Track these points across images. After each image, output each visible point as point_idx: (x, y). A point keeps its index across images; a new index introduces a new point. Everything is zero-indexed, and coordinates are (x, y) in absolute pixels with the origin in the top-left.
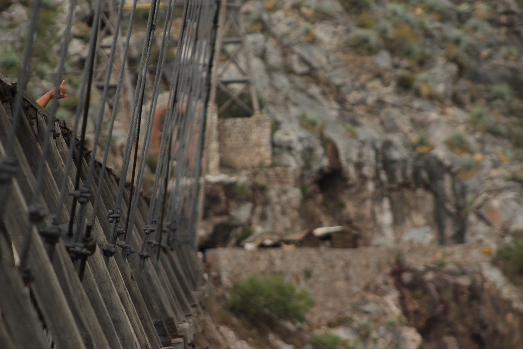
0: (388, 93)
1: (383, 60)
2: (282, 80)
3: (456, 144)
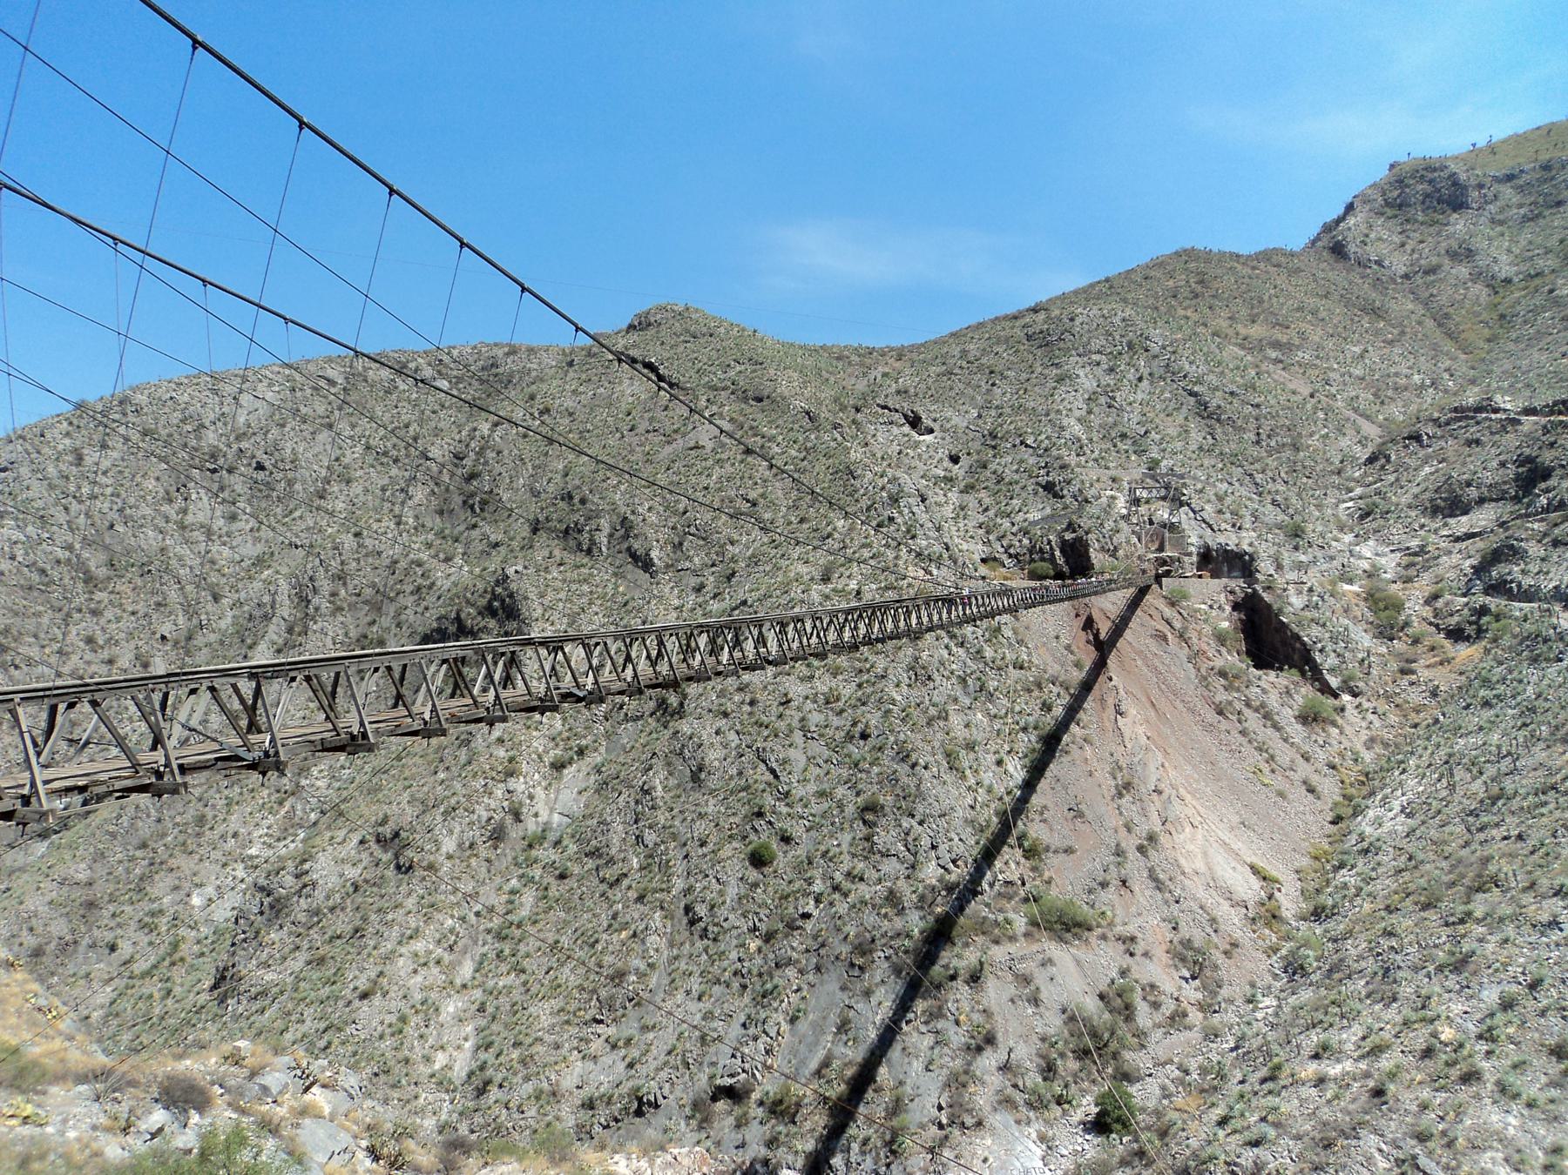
0: (1229, 527)
1: (1228, 516)
3: (1251, 545)
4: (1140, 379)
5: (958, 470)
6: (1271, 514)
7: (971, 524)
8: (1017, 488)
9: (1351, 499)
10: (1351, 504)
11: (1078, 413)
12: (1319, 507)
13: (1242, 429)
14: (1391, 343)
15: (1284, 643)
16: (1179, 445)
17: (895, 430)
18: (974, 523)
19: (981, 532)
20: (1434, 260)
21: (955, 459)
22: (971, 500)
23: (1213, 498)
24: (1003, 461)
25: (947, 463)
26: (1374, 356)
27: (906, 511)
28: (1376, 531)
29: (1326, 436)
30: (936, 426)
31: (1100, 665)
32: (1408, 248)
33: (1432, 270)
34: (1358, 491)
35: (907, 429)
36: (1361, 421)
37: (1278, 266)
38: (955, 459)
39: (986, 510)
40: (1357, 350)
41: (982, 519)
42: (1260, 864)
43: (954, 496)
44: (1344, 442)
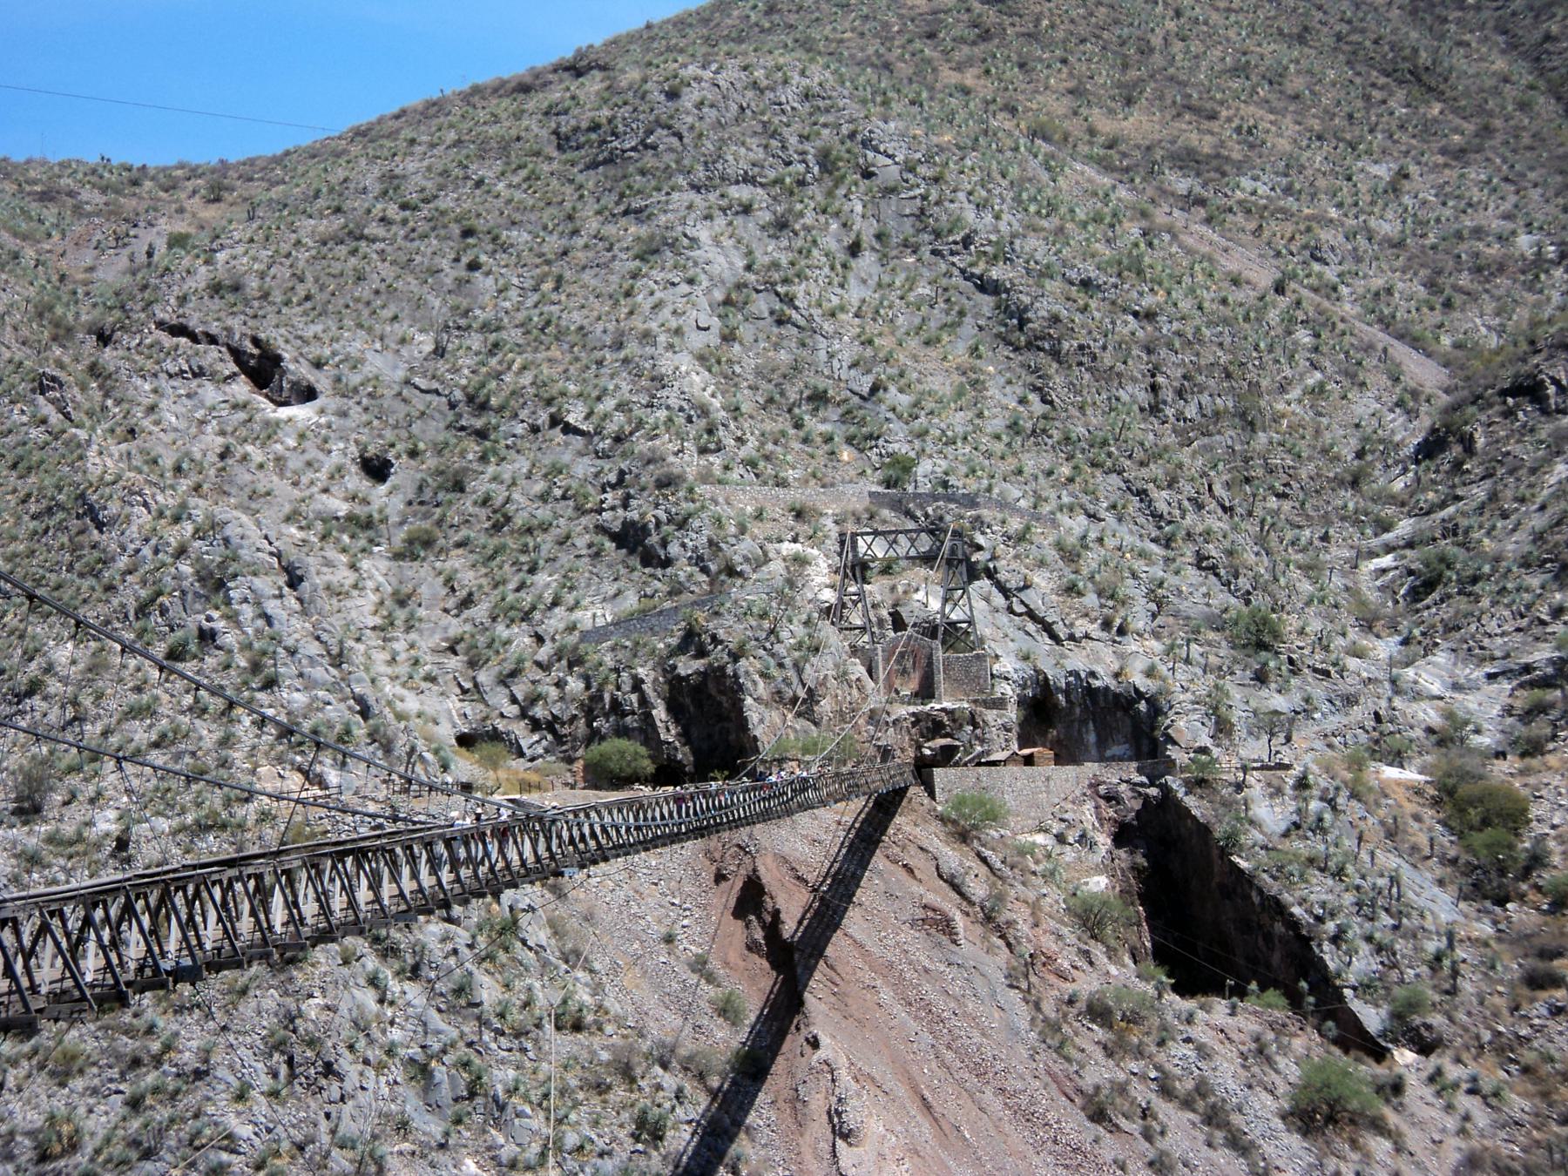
1: (1091, 600)
2: (1004, 619)
3: (1150, 673)
4: (854, 249)
6: (1197, 593)
7: (427, 642)
8: (546, 542)
9: (1389, 549)
10: (1387, 561)
11: (697, 341)
14: (1460, 154)
16: (958, 421)
17: (210, 393)
18: (437, 640)
19: (454, 662)
21: (376, 469)
22: (424, 577)
23: (1052, 554)
24: (507, 471)
25: (356, 481)
26: (1422, 186)
27: (247, 612)
28: (1450, 628)
29: (1319, 391)
30: (322, 381)
35: (241, 389)
40: (1383, 171)
41: (455, 626)
43: (377, 568)
44: (1364, 405)
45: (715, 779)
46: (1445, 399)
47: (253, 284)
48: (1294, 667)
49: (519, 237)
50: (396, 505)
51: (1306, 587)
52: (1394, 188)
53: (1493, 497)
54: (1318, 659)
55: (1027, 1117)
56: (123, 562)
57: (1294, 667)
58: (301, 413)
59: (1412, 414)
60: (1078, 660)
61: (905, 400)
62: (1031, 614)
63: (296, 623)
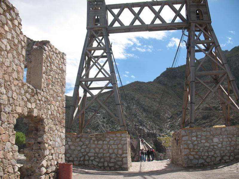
4: (134, 104)
5: (105, 120)
6: (157, 127)
9: (169, 124)
12: (164, 126)
13: (151, 113)
14: (171, 98)
15: (162, 148)
16: (142, 116)
20: (175, 84)
21: (104, 118)
26: (168, 100)
27: (100, 128)
28: (173, 130)
29: (163, 114)
30: (100, 112)
31: (69, 153)
32: (171, 82)
33: (175, 86)
34: (169, 123)
36: (168, 111)
37: (151, 84)
38: (104, 118)
39: (111, 127)
40: (166, 99)
42: (238, 89)
44: (166, 115)
45: (231, 118)
46: (171, 115)
47: (95, 106)
48: (164, 132)
49: (112, 103)
50: (105, 121)
51: (164, 127)
52: (166, 100)
53: (175, 121)
54: (165, 131)
55: (225, 119)
56: (92, 124)
57: (164, 132)
58: (99, 114)
59: (169, 115)
60: (150, 131)
61: (138, 114)
62: (147, 128)
63: (104, 129)
